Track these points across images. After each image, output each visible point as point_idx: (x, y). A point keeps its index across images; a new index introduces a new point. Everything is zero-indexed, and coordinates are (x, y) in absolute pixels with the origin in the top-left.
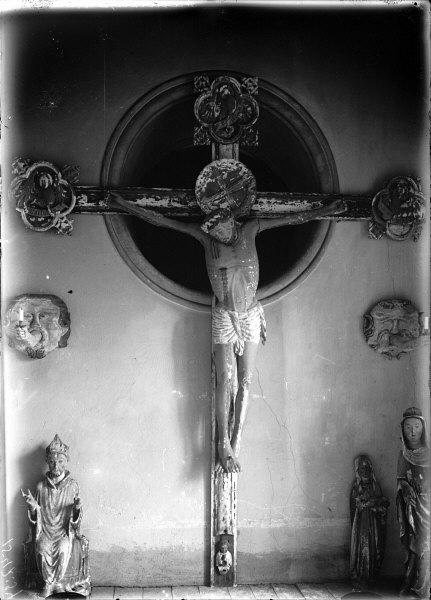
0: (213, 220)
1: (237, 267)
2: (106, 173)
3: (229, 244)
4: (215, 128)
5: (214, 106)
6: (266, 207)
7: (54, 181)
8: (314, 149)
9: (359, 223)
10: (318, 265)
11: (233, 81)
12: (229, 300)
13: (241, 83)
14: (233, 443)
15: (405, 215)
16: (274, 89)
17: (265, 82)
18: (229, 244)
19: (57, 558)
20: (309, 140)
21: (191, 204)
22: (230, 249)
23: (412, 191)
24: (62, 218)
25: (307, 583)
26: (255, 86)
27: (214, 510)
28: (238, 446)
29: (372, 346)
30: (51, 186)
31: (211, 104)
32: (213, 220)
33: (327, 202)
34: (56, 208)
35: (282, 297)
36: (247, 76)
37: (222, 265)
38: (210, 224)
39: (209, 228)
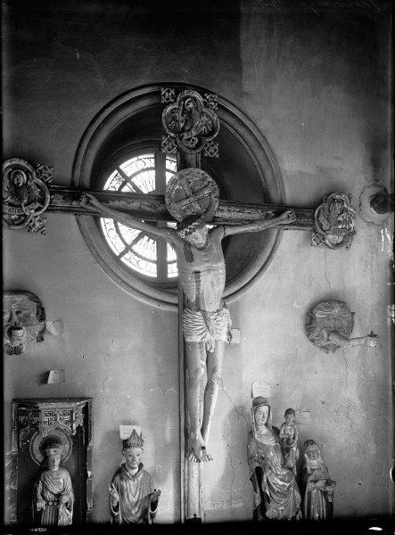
0: (191, 227)
1: (209, 270)
2: (78, 173)
3: (201, 249)
4: (181, 139)
5: (179, 115)
6: (226, 215)
7: (28, 179)
8: (264, 164)
9: (303, 232)
10: (270, 267)
11: (197, 95)
12: (201, 301)
13: (204, 97)
14: (203, 431)
15: (340, 227)
16: (231, 106)
17: (222, 98)
18: (201, 249)
19: (282, 220)
20: (260, 155)
21: (160, 209)
22: (202, 253)
23: (345, 206)
24: (36, 217)
25: (270, 202)
26: (215, 102)
27: (184, 497)
28: (207, 435)
29: (312, 341)
30: (25, 184)
31: (177, 115)
32: (191, 227)
33: (278, 214)
34: (31, 206)
35: (239, 297)
36: (209, 92)
37: (197, 269)
38: (188, 231)
39: (186, 234)
